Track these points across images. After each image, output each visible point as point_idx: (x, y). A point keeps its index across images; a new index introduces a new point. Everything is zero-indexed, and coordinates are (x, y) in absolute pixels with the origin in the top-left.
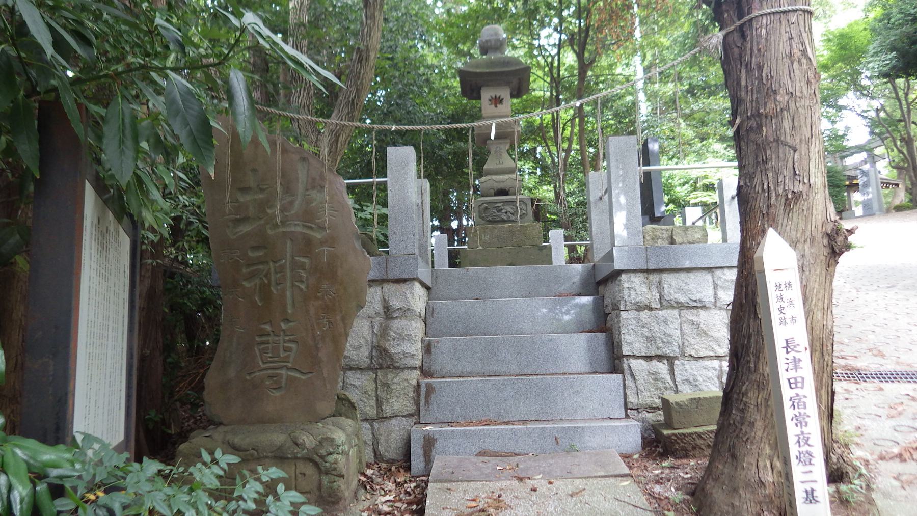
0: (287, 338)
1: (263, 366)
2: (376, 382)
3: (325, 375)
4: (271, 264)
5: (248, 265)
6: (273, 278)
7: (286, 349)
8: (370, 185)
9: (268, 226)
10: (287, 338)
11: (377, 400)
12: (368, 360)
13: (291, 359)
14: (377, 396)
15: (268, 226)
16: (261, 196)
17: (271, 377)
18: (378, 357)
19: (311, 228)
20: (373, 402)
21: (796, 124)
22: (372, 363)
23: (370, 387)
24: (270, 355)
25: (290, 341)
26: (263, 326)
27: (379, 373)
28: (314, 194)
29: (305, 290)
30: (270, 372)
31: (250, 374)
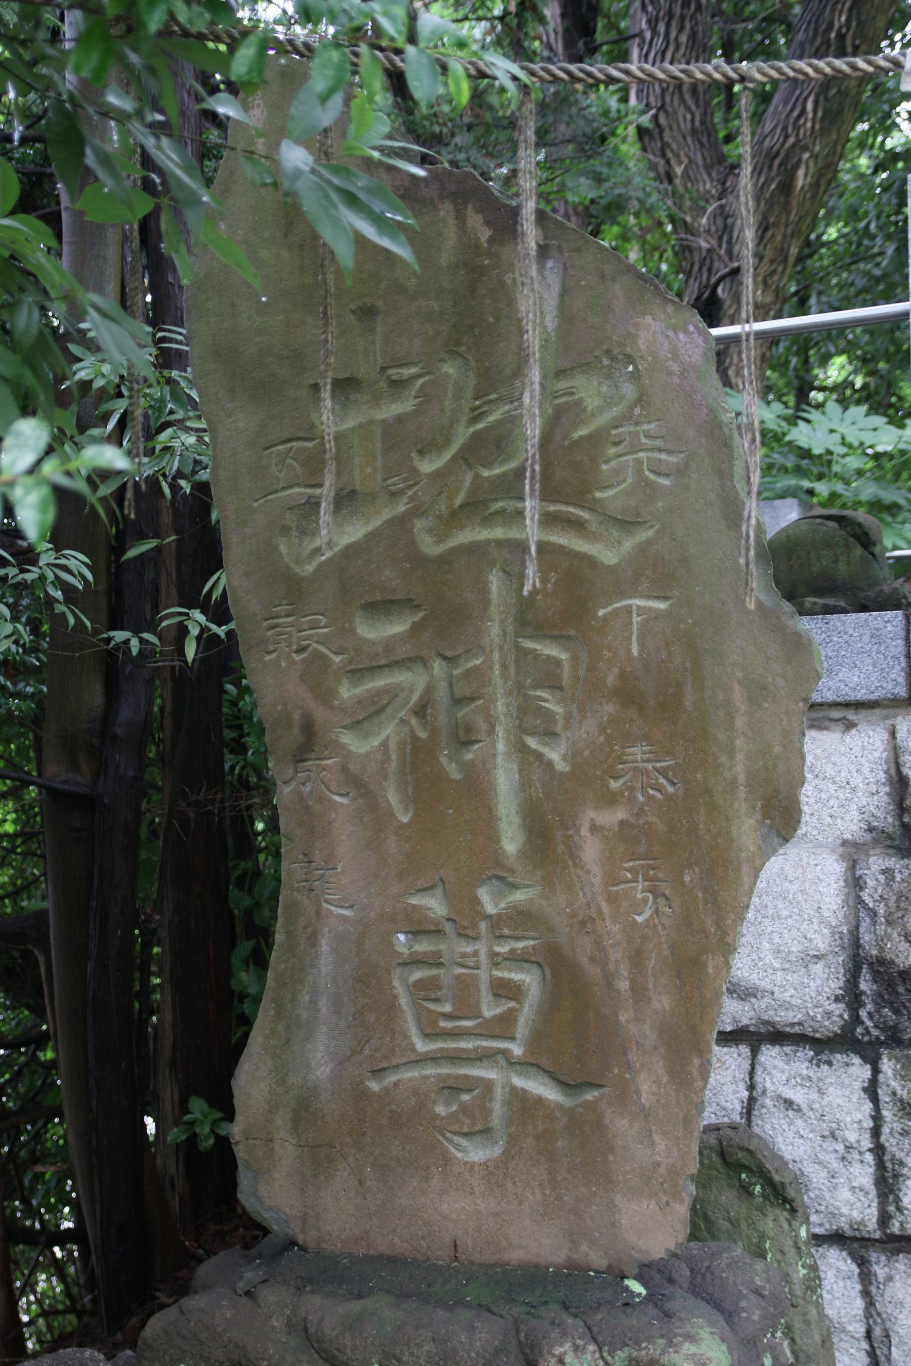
0: (503, 949)
1: (421, 1046)
2: (875, 1099)
3: (646, 1099)
4: (438, 666)
5: (357, 674)
6: (443, 719)
7: (505, 990)
8: (762, 313)
9: (420, 524)
10: (503, 949)
11: (881, 1165)
12: (839, 1009)
13: (522, 1028)
14: (878, 1150)
15: (420, 524)
16: (396, 409)
17: (452, 1088)
18: (879, 1000)
19: (577, 525)
20: (863, 1174)
21: (432, 928)
22: (856, 1020)
23: (854, 1113)
24: (447, 1008)
25: (515, 958)
26: (415, 901)
27: (887, 1066)
28: (589, 390)
29: (561, 766)
30: (445, 1070)
31: (377, 1073)
